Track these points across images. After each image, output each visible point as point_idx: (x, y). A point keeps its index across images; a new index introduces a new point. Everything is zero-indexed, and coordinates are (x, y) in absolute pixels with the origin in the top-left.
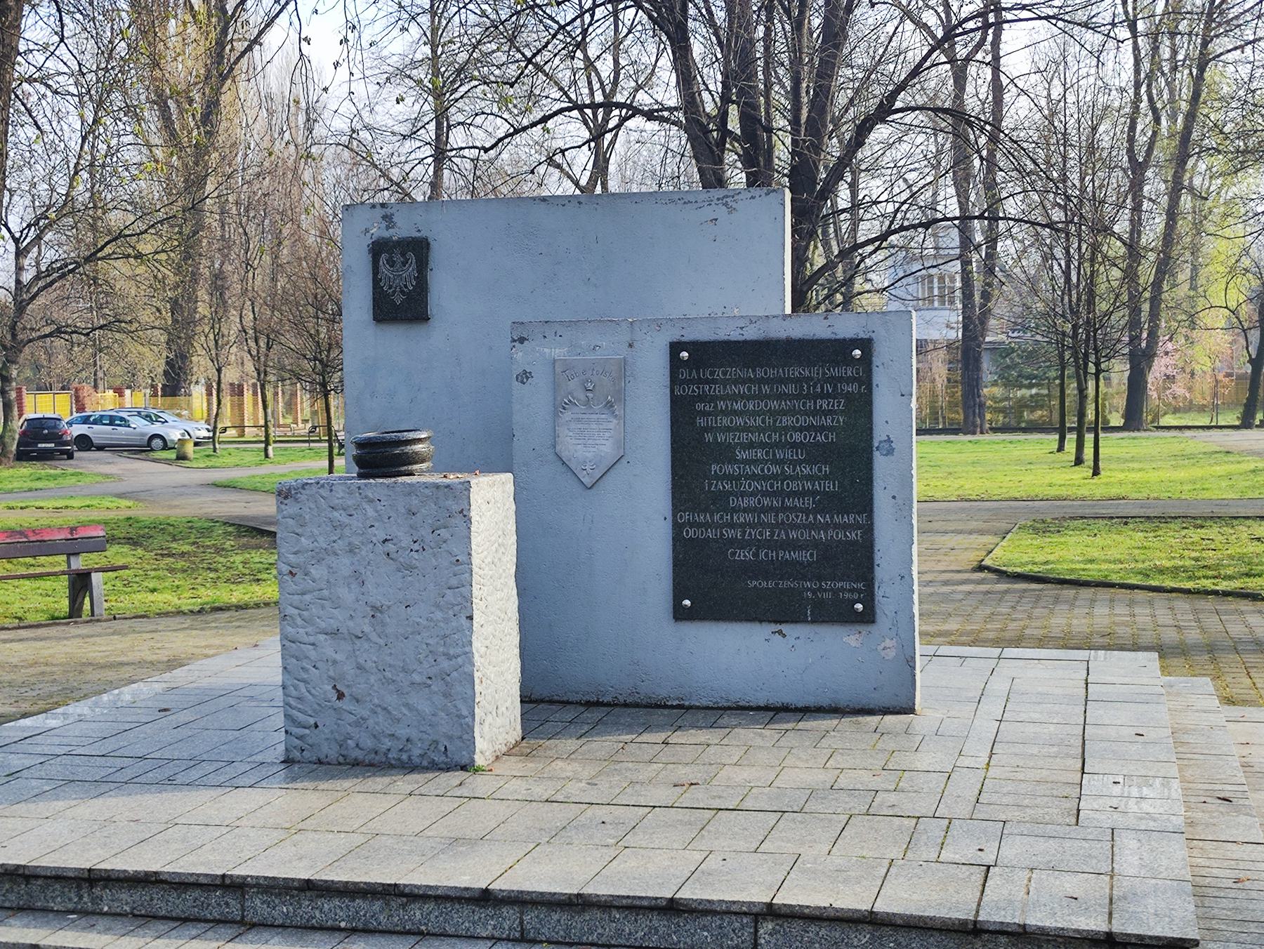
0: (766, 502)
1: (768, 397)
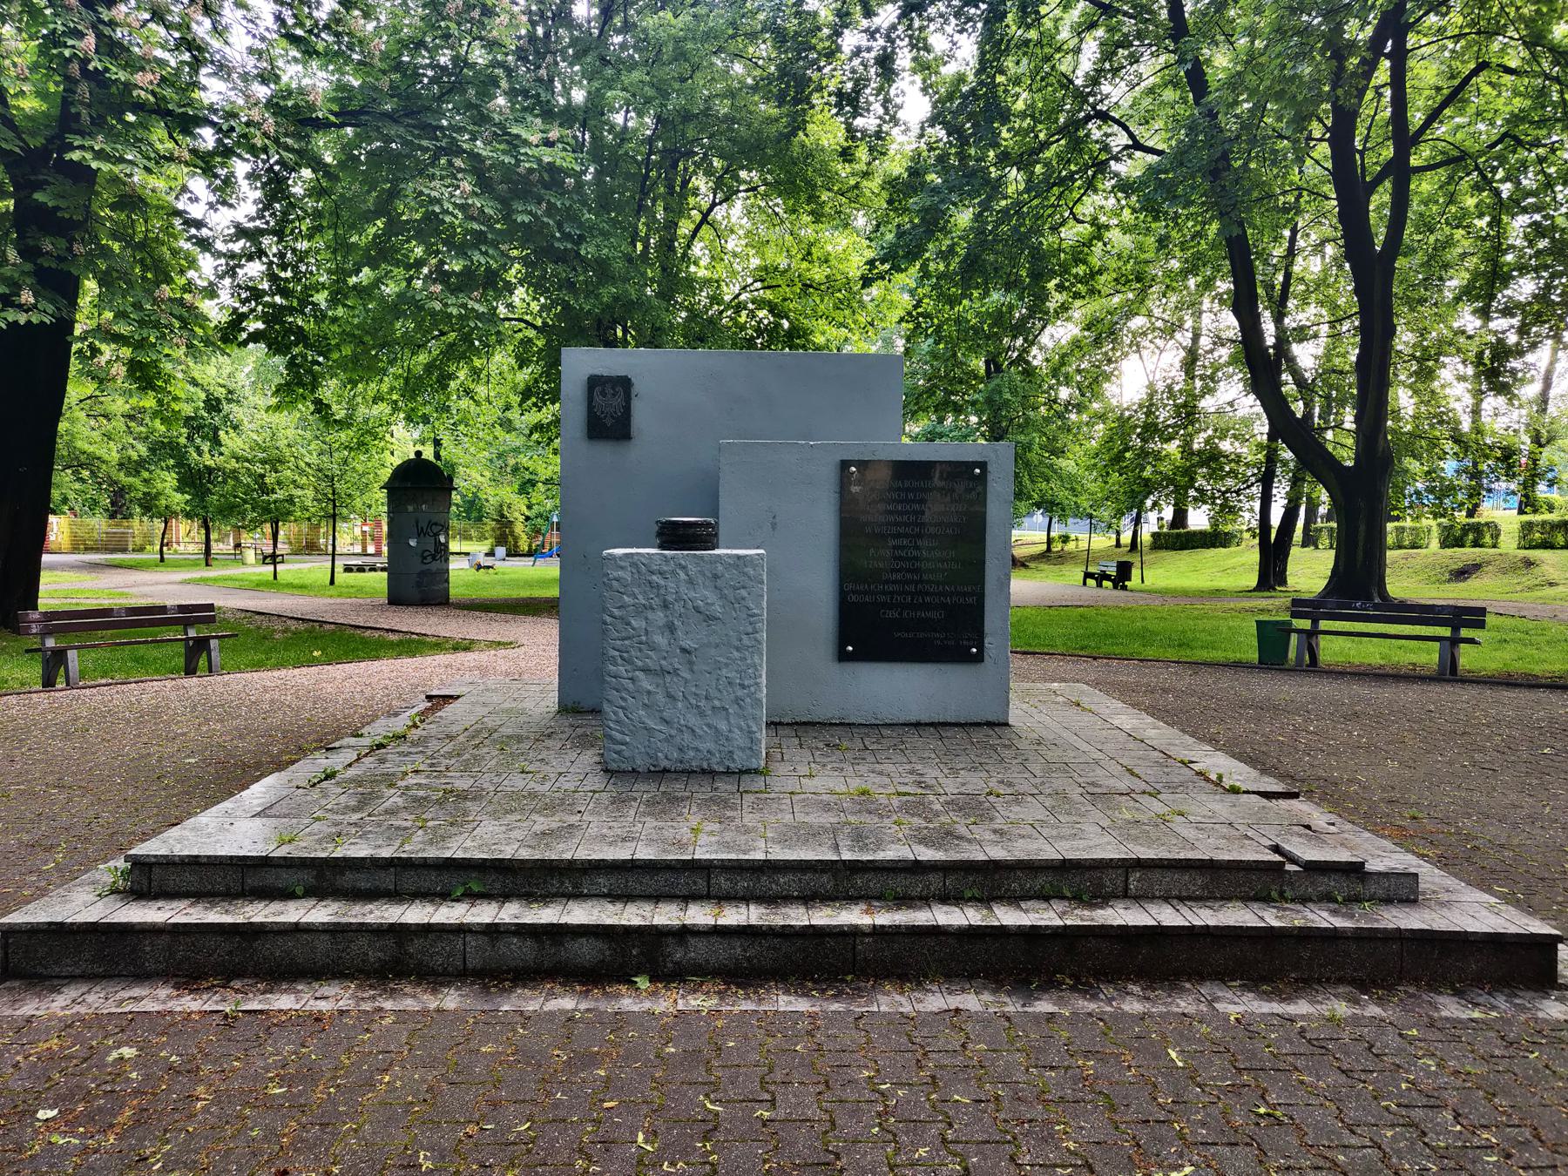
0: (909, 576)
1: (913, 501)
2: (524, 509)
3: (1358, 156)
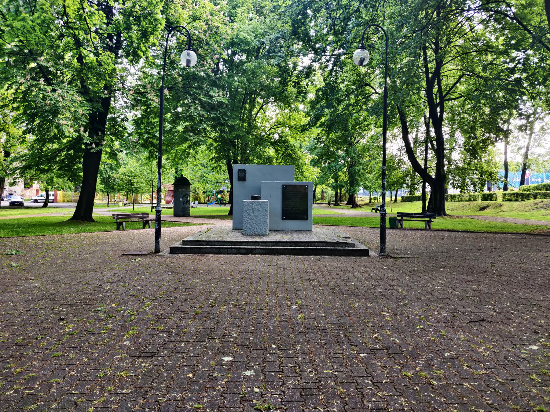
2: (203, 189)
3: (434, 96)
